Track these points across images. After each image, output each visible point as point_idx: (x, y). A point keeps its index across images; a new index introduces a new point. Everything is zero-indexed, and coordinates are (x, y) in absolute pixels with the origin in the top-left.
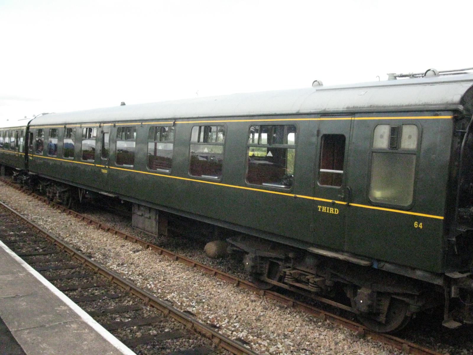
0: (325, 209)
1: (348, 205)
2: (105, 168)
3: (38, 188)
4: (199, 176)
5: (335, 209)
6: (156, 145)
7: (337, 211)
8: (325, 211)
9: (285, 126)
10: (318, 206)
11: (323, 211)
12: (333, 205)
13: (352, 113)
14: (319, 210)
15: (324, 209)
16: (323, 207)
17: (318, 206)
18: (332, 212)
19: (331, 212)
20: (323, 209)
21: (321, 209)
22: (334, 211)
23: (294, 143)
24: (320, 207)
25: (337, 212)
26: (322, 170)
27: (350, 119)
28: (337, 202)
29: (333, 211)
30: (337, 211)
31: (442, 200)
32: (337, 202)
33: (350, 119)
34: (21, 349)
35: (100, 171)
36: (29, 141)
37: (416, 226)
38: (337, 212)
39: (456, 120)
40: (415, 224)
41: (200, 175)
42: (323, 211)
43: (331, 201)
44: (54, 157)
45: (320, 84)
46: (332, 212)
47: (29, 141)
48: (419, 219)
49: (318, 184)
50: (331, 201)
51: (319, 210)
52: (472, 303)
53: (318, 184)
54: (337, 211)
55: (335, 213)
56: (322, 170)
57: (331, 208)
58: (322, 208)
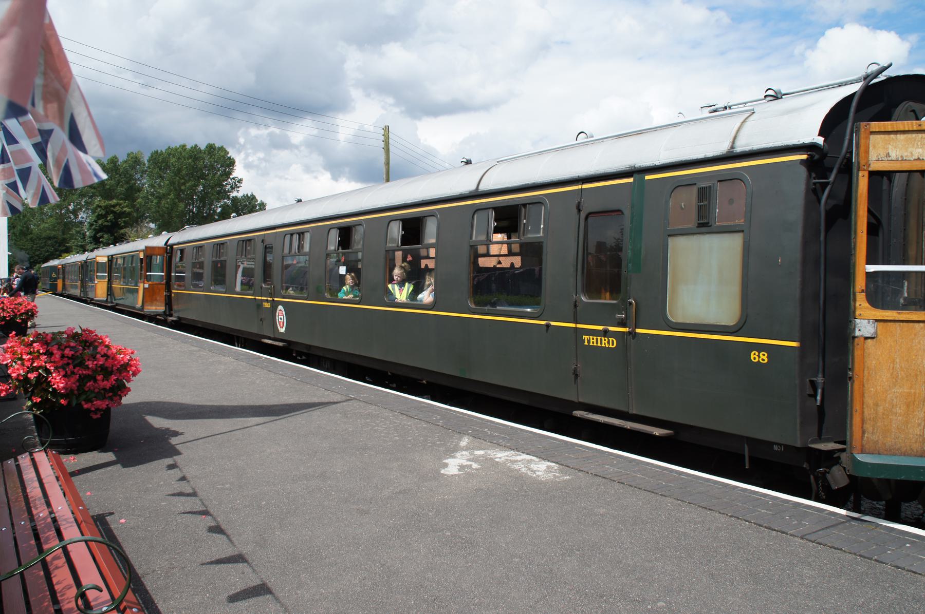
0: (595, 341)
2: (267, 301)
4: (493, 307)
5: (611, 339)
6: (428, 252)
8: (595, 344)
9: (527, 205)
10: (584, 336)
11: (591, 344)
12: (605, 333)
13: (858, 144)
14: (586, 343)
16: (591, 337)
17: (584, 336)
18: (605, 344)
19: (603, 345)
20: (591, 341)
21: (589, 341)
24: (586, 337)
25: (613, 345)
26: (148, 274)
27: (580, 187)
28: (611, 329)
29: (606, 344)
30: (613, 341)
31: (791, 310)
32: (611, 329)
33: (580, 187)
37: (755, 358)
38: (613, 345)
39: (809, 164)
40: (752, 356)
41: (494, 305)
42: (591, 344)
43: (600, 328)
44: (132, 286)
46: (605, 344)
48: (760, 348)
49: (583, 298)
50: (600, 328)
53: (583, 298)
54: (613, 341)
55: (611, 346)
56: (148, 274)
58: (590, 338)
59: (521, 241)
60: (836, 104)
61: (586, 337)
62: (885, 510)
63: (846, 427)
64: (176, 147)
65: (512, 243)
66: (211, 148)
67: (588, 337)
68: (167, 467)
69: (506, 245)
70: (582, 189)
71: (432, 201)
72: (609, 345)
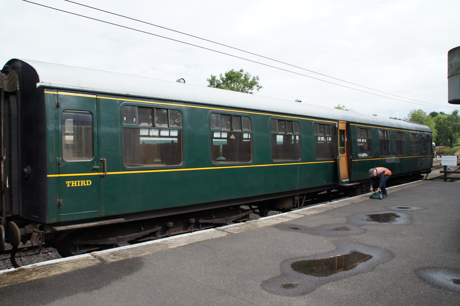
1: (340, 151)
3: (58, 202)
5: (87, 181)
7: (89, 183)
10: (67, 182)
14: (68, 186)
15: (74, 184)
16: (73, 182)
17: (67, 182)
21: (71, 184)
22: (86, 183)
23: (282, 143)
24: (68, 182)
25: (89, 183)
29: (84, 184)
30: (89, 182)
34: (196, 242)
35: (227, 158)
36: (437, 162)
42: (73, 185)
45: (247, 93)
47: (437, 162)
51: (68, 186)
52: (1, 277)
54: (89, 182)
57: (82, 181)
58: (71, 182)
59: (368, 138)
60: (28, 64)
61: (68, 182)
62: (11, 262)
63: (348, 174)
64: (445, 118)
65: (215, 132)
66: (419, 110)
67: (70, 182)
68: (143, 263)
69: (177, 131)
70: (57, 94)
71: (66, 89)
72: (86, 184)
